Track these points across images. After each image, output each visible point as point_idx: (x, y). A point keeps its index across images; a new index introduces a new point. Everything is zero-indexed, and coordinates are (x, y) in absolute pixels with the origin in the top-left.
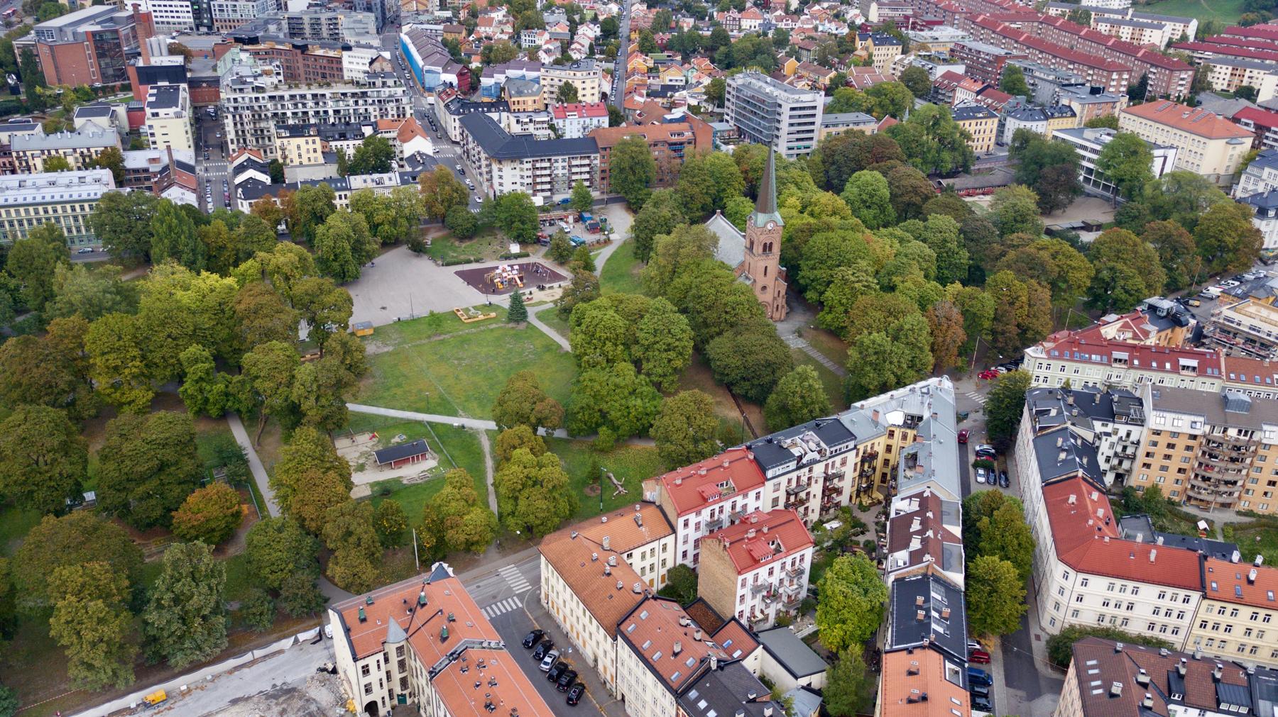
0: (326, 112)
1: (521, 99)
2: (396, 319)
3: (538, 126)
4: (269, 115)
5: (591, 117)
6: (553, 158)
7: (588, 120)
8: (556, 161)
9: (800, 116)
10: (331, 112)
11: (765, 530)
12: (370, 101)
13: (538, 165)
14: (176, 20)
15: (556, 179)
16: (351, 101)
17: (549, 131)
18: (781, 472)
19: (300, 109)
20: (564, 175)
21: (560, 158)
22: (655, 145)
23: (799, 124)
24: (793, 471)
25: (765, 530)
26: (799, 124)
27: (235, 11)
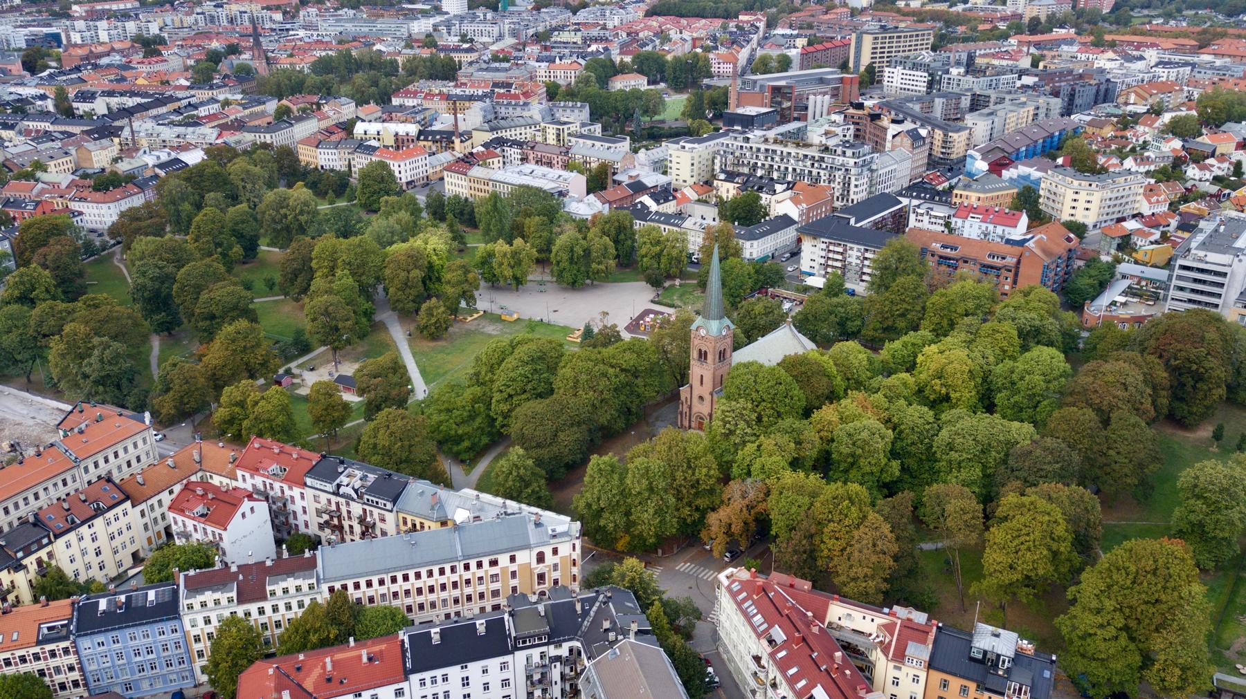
0: (787, 169)
1: (965, 193)
2: (539, 318)
3: (933, 220)
4: (746, 162)
5: (996, 223)
6: (849, 245)
7: (991, 227)
8: (851, 249)
9: (1195, 280)
10: (790, 169)
11: (210, 496)
12: (824, 166)
13: (831, 248)
14: (914, 88)
15: (849, 267)
16: (809, 163)
17: (942, 228)
18: (318, 486)
19: (769, 162)
20: (857, 265)
21: (856, 247)
22: (966, 262)
23: (1193, 291)
24: (329, 493)
25: (210, 496)
26: (1193, 291)
27: (959, 85)
